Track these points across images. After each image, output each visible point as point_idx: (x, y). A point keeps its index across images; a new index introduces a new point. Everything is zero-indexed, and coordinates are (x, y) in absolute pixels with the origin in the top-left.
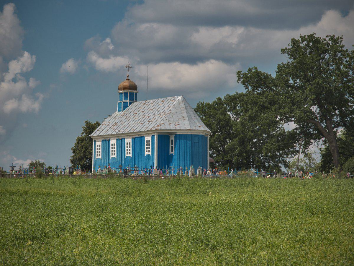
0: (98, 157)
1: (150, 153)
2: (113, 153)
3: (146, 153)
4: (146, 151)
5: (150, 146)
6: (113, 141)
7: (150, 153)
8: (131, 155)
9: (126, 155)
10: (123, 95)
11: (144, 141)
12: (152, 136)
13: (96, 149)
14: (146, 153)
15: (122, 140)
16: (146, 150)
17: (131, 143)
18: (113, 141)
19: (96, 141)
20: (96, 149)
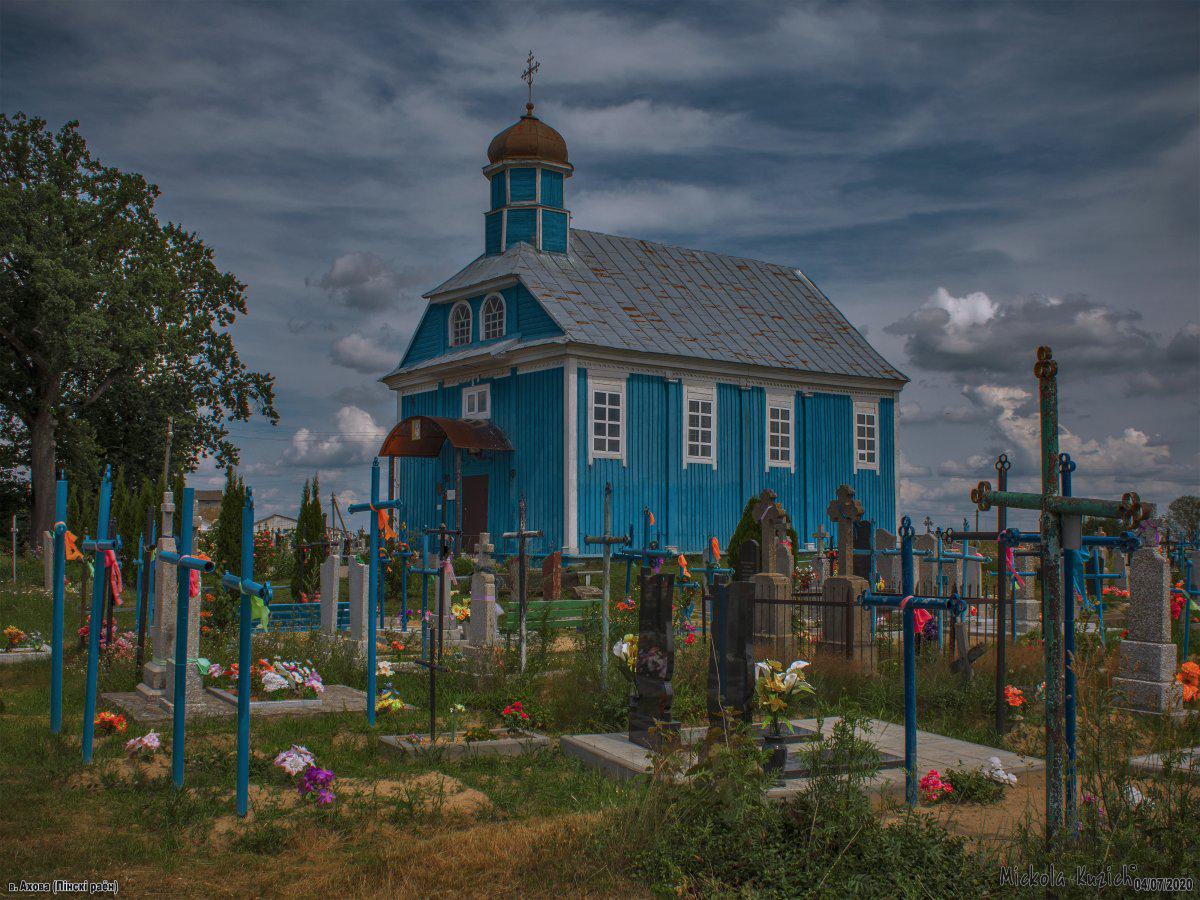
0: (780, 464)
1: (875, 466)
2: (779, 448)
3: (859, 465)
4: (856, 457)
5: (877, 439)
6: (780, 400)
7: (875, 466)
8: (790, 464)
9: (769, 463)
10: (539, 178)
11: (850, 413)
12: (883, 401)
13: (591, 413)
14: (859, 465)
15: (668, 390)
16: (857, 452)
17: (792, 416)
18: (699, 392)
19: (589, 372)
20: (591, 413)
